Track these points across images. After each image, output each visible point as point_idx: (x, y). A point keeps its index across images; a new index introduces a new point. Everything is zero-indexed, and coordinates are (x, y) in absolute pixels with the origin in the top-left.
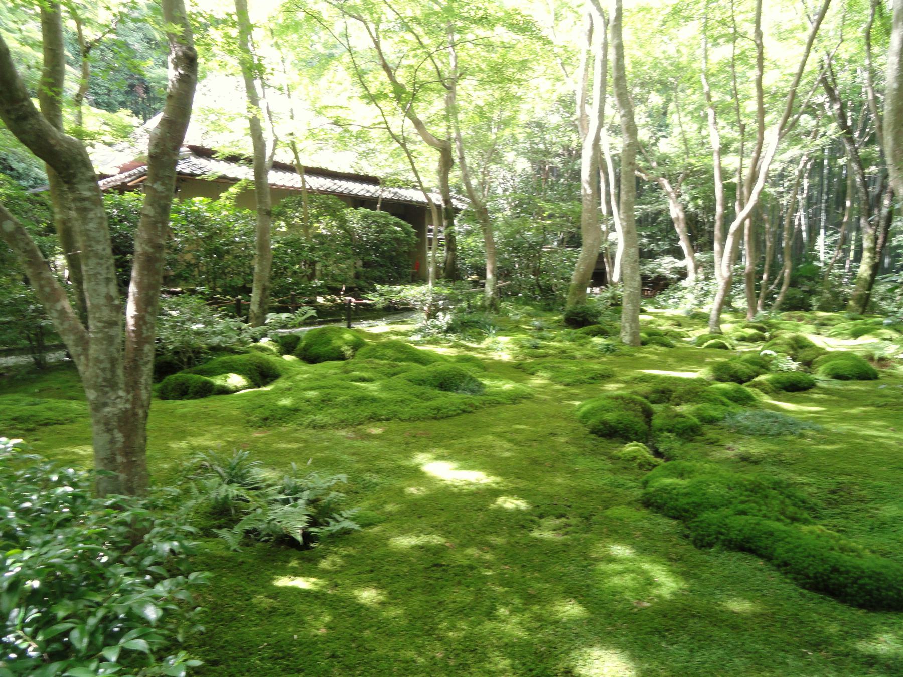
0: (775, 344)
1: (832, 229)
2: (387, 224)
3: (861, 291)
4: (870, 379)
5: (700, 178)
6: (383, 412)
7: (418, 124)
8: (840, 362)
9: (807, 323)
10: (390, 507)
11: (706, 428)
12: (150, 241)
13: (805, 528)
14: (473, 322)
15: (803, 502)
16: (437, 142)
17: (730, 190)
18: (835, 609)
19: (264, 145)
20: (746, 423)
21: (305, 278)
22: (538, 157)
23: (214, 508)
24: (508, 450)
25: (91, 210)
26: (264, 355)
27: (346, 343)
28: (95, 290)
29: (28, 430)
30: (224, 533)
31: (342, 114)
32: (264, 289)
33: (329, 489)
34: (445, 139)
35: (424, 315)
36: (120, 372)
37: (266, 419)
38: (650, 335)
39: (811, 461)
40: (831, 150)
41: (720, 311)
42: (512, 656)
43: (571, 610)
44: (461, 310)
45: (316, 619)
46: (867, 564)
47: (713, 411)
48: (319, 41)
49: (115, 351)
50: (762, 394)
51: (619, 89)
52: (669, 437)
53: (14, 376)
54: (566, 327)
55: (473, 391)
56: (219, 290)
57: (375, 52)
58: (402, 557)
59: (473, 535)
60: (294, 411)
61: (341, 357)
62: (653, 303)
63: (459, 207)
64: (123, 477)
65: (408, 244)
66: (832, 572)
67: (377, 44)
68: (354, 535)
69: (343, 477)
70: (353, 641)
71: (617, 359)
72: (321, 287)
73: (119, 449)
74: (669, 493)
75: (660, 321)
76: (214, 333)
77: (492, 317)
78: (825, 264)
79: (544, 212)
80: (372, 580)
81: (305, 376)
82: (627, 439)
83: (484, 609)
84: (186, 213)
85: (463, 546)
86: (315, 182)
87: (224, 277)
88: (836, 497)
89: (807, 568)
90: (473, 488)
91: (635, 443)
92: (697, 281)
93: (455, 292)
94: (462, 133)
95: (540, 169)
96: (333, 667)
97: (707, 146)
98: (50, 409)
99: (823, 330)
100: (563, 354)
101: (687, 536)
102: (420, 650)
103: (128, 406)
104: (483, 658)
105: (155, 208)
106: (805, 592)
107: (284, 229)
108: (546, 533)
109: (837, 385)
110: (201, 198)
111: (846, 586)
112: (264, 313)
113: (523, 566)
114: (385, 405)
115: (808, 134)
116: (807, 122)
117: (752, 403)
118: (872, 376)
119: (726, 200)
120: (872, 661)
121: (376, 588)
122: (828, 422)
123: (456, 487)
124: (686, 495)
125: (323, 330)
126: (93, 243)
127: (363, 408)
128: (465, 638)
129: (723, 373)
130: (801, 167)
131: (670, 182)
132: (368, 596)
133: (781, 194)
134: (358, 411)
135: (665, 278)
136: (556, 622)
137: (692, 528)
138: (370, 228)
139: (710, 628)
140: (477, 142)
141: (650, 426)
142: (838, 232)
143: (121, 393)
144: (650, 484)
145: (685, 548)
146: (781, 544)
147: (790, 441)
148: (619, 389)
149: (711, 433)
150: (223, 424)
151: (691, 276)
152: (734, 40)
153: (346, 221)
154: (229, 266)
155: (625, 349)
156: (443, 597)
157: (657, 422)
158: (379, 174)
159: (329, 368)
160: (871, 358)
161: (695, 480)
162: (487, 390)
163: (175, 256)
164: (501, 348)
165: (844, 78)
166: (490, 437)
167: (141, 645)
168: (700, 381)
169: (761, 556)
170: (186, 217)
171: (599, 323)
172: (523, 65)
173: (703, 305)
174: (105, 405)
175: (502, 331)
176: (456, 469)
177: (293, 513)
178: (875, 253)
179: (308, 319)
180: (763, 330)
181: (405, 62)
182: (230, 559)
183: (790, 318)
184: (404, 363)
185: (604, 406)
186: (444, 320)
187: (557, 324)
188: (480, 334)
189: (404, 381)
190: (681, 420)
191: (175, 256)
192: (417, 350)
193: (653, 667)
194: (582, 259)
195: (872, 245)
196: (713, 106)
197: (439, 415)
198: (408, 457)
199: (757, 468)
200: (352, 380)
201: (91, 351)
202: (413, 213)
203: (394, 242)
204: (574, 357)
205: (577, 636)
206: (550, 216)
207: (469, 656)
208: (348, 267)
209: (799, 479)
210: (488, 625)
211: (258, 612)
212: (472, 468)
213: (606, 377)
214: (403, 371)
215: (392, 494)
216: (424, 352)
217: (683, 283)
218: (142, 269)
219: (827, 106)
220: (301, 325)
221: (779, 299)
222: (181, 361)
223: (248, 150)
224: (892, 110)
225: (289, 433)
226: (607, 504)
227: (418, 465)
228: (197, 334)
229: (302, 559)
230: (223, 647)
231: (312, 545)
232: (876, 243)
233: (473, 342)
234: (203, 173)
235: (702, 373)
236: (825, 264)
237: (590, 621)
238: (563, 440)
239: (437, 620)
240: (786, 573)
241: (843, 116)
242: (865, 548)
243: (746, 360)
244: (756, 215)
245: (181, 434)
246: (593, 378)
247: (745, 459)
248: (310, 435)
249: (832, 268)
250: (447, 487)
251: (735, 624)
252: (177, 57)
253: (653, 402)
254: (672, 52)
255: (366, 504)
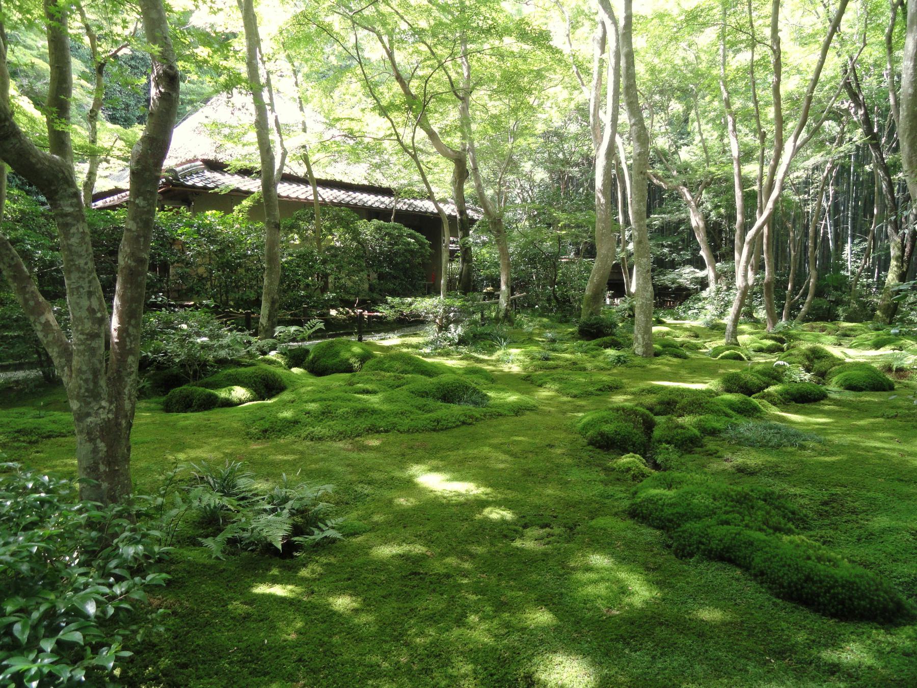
0: (790, 355)
1: (860, 237)
2: (401, 236)
3: (888, 301)
4: (884, 390)
5: (720, 186)
6: (382, 424)
7: (432, 135)
8: (854, 373)
9: (829, 334)
10: (376, 518)
11: (707, 439)
12: (132, 255)
13: (786, 538)
14: (486, 334)
15: (793, 513)
16: (451, 153)
17: (751, 199)
18: (806, 618)
19: (272, 158)
20: (748, 434)
21: (319, 291)
22: (557, 168)
23: (204, 518)
24: (502, 462)
25: (74, 225)
26: (271, 368)
27: (354, 355)
28: (78, 304)
29: (30, 442)
30: (209, 542)
31: (355, 126)
32: (273, 302)
33: (318, 500)
34: (459, 150)
35: (435, 327)
36: (103, 383)
37: (265, 431)
38: (664, 346)
39: (807, 471)
40: (857, 156)
41: (736, 321)
42: (475, 661)
43: (542, 617)
44: (475, 322)
45: (288, 625)
46: (841, 573)
47: (714, 422)
48: (332, 54)
49: (96, 362)
50: (770, 405)
51: (629, 98)
52: (667, 449)
53: (22, 390)
54: (580, 339)
55: (475, 403)
56: (232, 303)
57: (388, 64)
58: (382, 566)
59: (454, 545)
60: (295, 422)
61: (349, 369)
62: (672, 314)
63: (476, 218)
64: (105, 485)
65: (422, 255)
66: (805, 581)
67: (390, 55)
68: (338, 544)
69: (330, 488)
70: (322, 646)
71: (628, 371)
72: (334, 299)
73: (101, 458)
74: (655, 503)
75: (678, 332)
76: (222, 347)
77: (506, 329)
78: (853, 273)
79: (559, 222)
80: (348, 588)
81: (309, 388)
82: (625, 451)
83: (454, 616)
84: (199, 227)
85: (446, 555)
86: (327, 194)
87: (236, 290)
88: (827, 508)
89: (782, 577)
90: (462, 499)
91: (631, 454)
92: (718, 291)
93: (467, 304)
94: (476, 144)
95: (559, 178)
96: (299, 670)
97: (728, 154)
98: (54, 422)
99: (845, 341)
100: (575, 366)
101: (669, 546)
102: (386, 656)
103: (111, 416)
104: (448, 663)
105: (137, 223)
106: (779, 601)
107: (297, 242)
108: (528, 543)
109: (850, 396)
110: (214, 212)
111: (818, 595)
112: (273, 326)
113: (500, 575)
114: (385, 417)
115: (832, 141)
116: (831, 127)
117: (758, 414)
118: (887, 387)
119: (745, 206)
120: (834, 669)
121: (351, 595)
122: (833, 434)
123: (445, 498)
124: (671, 505)
125: (332, 342)
126: (75, 257)
127: (362, 420)
128: (431, 643)
129: (733, 384)
130: (825, 174)
131: (690, 191)
132: (342, 603)
133: (806, 202)
134: (357, 422)
135: (686, 289)
136: (523, 630)
137: (675, 540)
138: (383, 240)
139: (676, 635)
140: (493, 150)
141: (650, 438)
142: (866, 240)
143: (104, 403)
144: (639, 495)
145: (667, 559)
146: (759, 553)
147: (790, 452)
148: (626, 400)
149: (711, 444)
150: (223, 437)
151: (712, 287)
152: (753, 46)
153: (360, 233)
154: (242, 279)
155: (637, 361)
156: (415, 604)
157: (657, 433)
158: (394, 185)
159: (336, 381)
160: (889, 369)
161: (681, 491)
162: (491, 402)
163: (188, 270)
164: (512, 360)
165: (869, 83)
166: (487, 449)
167: (77, 637)
168: (709, 393)
169: (739, 566)
170: (199, 230)
171: (614, 335)
172: (539, 75)
173: (720, 317)
174: (88, 415)
175: (513, 343)
176: (448, 480)
177: (275, 522)
178: (902, 262)
179: (316, 332)
180: (782, 341)
181: (420, 73)
182: (211, 567)
183: (813, 329)
184: (410, 376)
185: (603, 417)
186: (456, 331)
187: (570, 336)
188: (492, 346)
189: (406, 393)
190: (683, 431)
191: (188, 270)
192: (425, 362)
193: (613, 672)
194: (598, 268)
195: (899, 253)
196: (734, 114)
197: (438, 427)
198: (402, 468)
199: (752, 479)
200: (359, 393)
201: (74, 363)
202: (428, 225)
203: (408, 252)
204: (585, 369)
205: (542, 642)
206: (565, 227)
207: (433, 661)
208: (362, 280)
209: (792, 490)
210: (456, 632)
211: (232, 618)
212: (464, 479)
213: (614, 388)
214: (407, 383)
215: (380, 504)
216: (432, 364)
217: (704, 294)
218: (125, 282)
219: (852, 111)
220: (310, 338)
221: (804, 309)
222: (188, 374)
223: (258, 165)
224: (907, 116)
225: (286, 445)
226: (593, 515)
227: (411, 476)
228: (203, 347)
229: (283, 567)
230: (193, 651)
231: (295, 554)
232: (903, 251)
233: (484, 354)
234: (217, 187)
235: (710, 384)
236: (853, 273)
237: (557, 629)
238: (559, 451)
239: (406, 626)
240: (762, 583)
241: (867, 122)
242: (843, 558)
243: (758, 371)
244: (772, 220)
245: (180, 446)
246: (600, 390)
247: (742, 470)
248: (307, 447)
249: (859, 276)
250: (437, 497)
251: (703, 632)
252: (158, 76)
253: (656, 414)
254: (691, 57)
255: (354, 514)
